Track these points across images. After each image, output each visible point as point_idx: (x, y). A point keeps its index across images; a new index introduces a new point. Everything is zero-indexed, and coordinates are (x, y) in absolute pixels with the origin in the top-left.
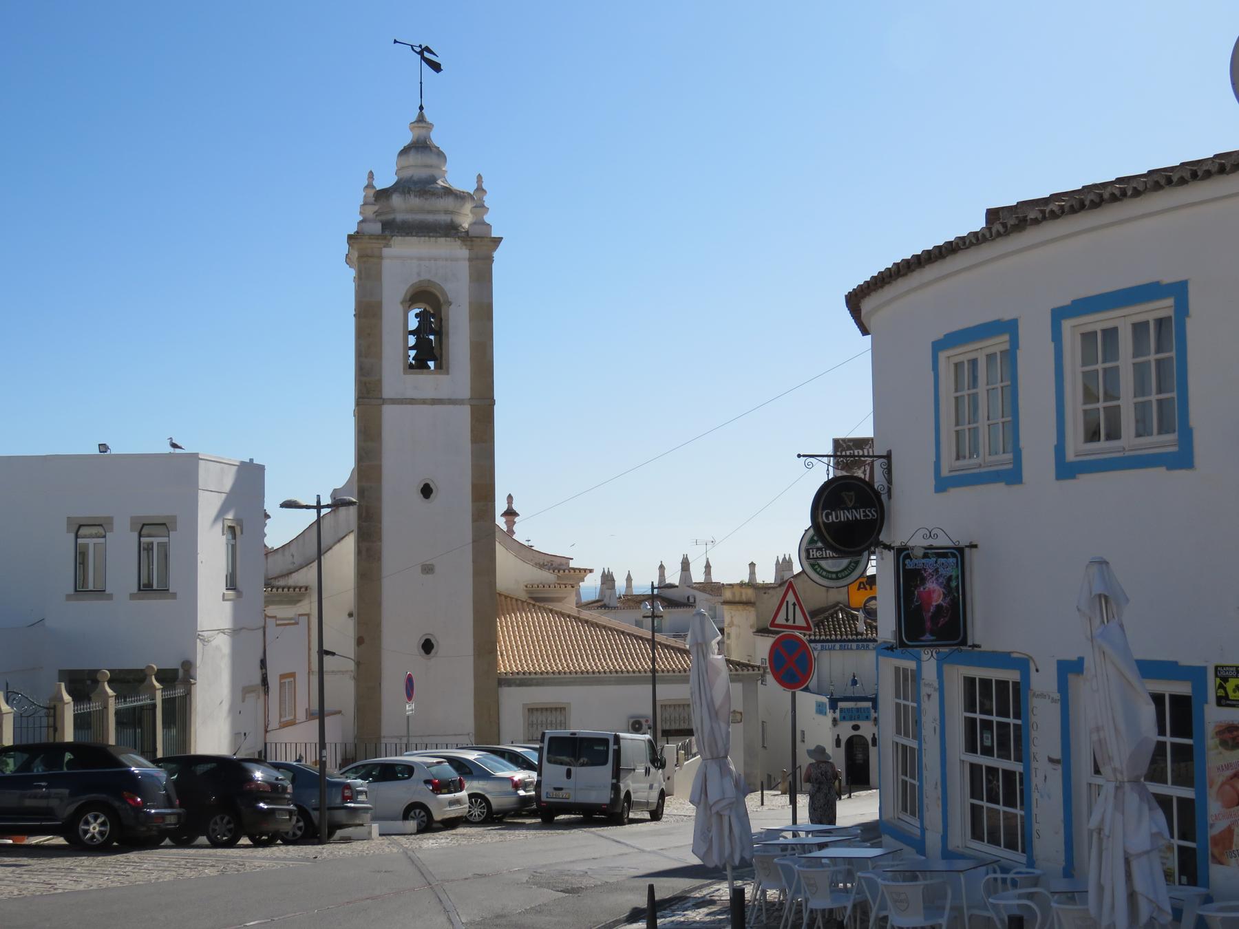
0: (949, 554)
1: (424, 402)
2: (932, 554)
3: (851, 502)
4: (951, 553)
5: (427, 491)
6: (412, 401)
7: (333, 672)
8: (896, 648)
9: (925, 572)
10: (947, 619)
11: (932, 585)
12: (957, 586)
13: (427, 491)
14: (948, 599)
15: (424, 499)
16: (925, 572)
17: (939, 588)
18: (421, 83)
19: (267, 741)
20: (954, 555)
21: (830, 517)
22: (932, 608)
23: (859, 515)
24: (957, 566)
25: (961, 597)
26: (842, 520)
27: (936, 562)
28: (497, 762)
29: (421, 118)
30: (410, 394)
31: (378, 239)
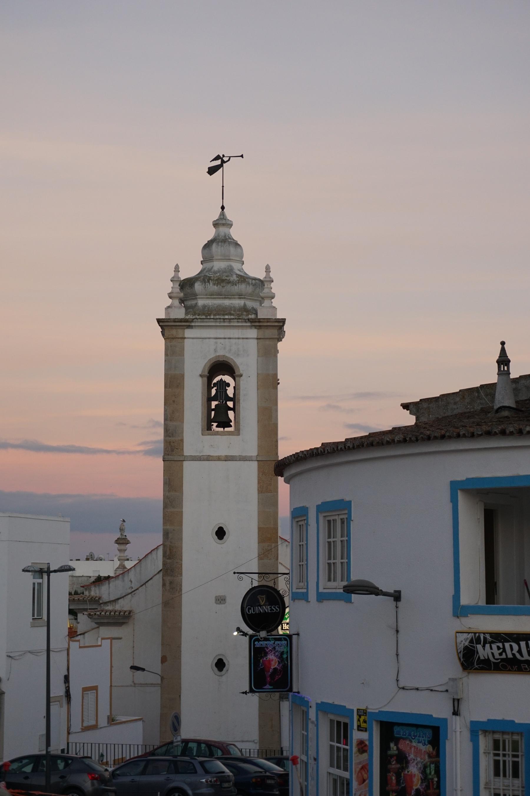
0: (283, 639)
1: (218, 459)
2: (272, 638)
3: (263, 602)
4: (284, 638)
5: (221, 533)
6: (208, 458)
7: (152, 684)
8: (248, 693)
9: (267, 649)
10: (280, 676)
11: (271, 656)
12: (287, 657)
13: (221, 533)
14: (281, 665)
15: (218, 541)
16: (267, 649)
17: (275, 658)
18: (223, 187)
19: (69, 742)
20: (286, 640)
21: (250, 610)
22: (271, 670)
23: (267, 609)
24: (287, 646)
25: (289, 663)
26: (257, 612)
27: (274, 643)
28: (522, 771)
29: (222, 217)
30: (207, 452)
31: (223, 299)
